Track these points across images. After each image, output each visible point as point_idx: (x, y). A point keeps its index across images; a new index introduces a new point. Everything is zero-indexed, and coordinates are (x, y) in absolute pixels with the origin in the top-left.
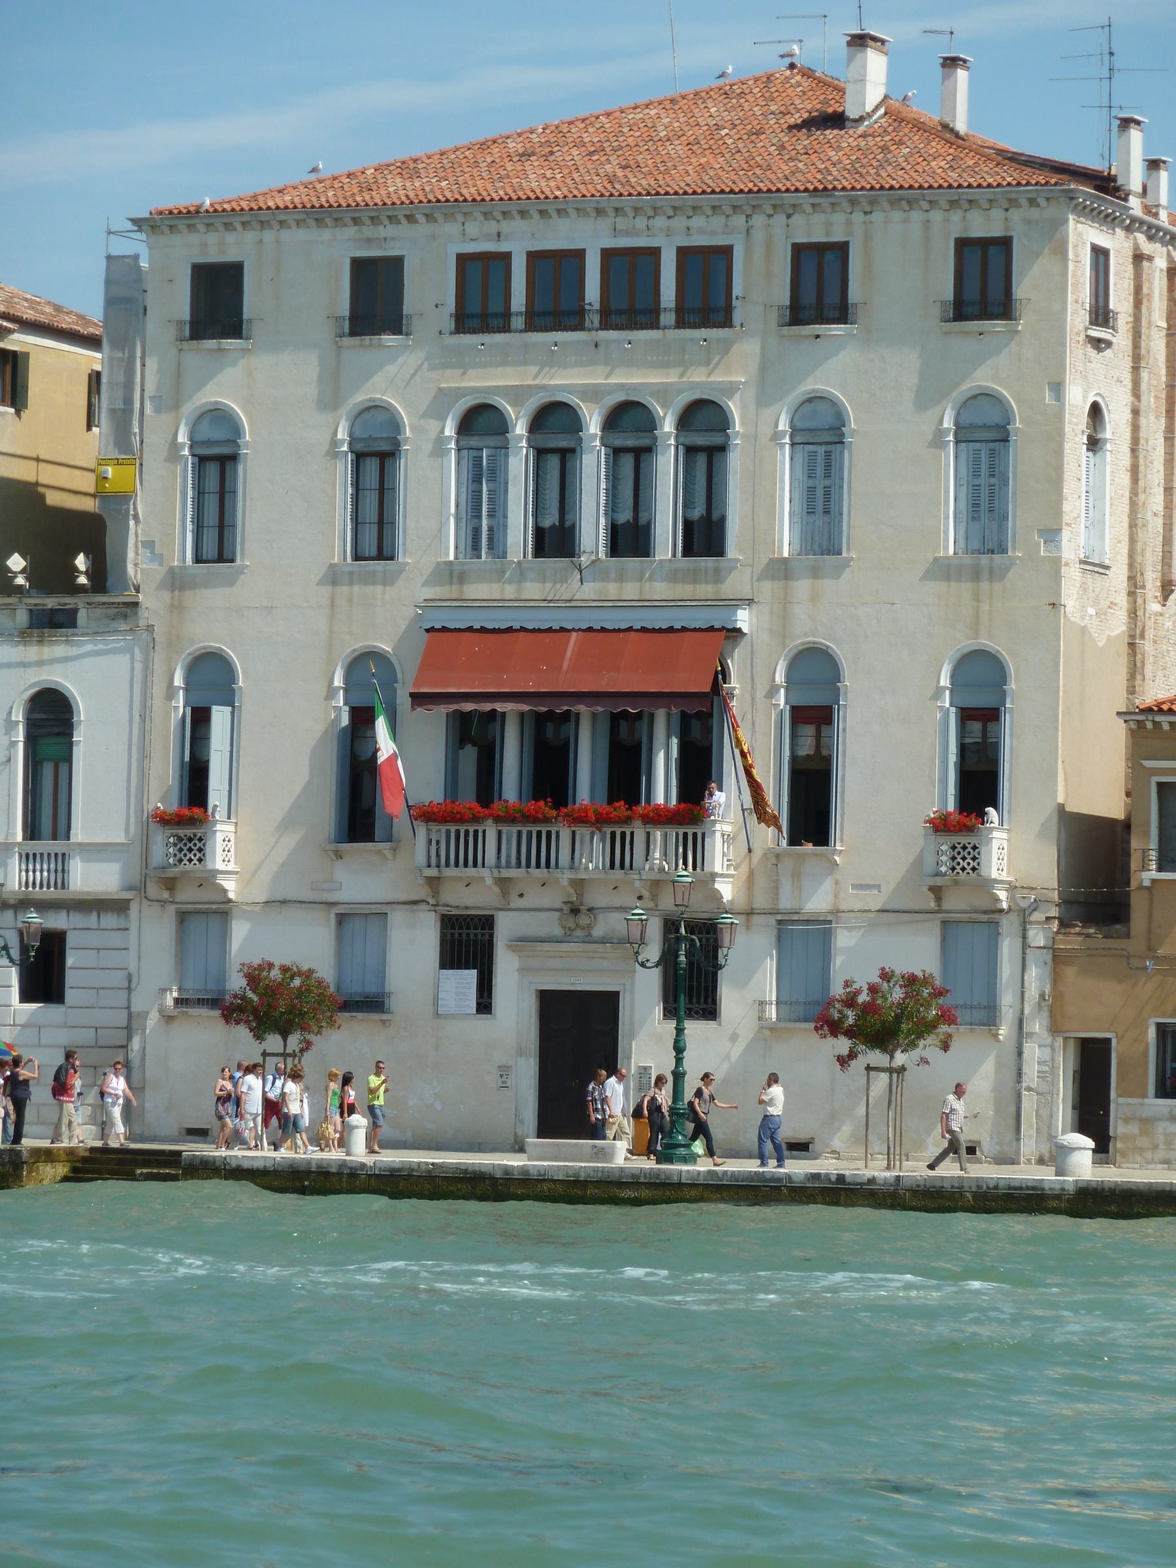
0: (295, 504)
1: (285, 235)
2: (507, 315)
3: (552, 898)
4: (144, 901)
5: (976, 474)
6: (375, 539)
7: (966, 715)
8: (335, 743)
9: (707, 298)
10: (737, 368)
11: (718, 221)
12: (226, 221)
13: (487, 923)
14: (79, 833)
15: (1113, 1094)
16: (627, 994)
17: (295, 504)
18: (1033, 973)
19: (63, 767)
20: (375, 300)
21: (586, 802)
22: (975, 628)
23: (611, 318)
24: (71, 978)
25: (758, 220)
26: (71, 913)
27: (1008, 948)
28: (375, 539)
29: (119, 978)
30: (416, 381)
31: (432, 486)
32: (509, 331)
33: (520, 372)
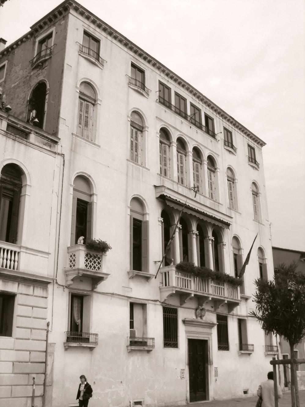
4: (55, 284)
8: (245, 291)
12: (252, 145)
16: (210, 341)
21: (238, 287)
24: (17, 321)
26: (20, 285)
29: (42, 324)
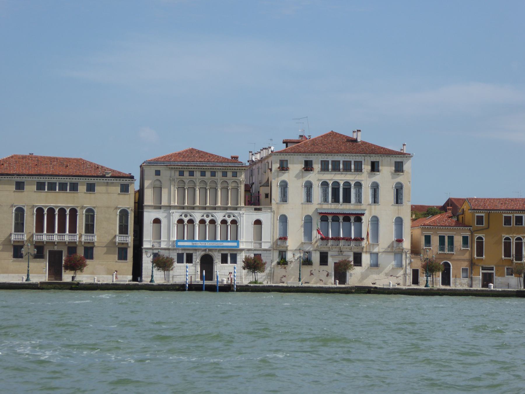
0: (296, 192)
6: (309, 198)
10: (366, 179)
11: (360, 158)
13: (327, 253)
17: (296, 192)
18: (407, 260)
22: (398, 214)
25: (366, 158)
27: (404, 256)
28: (309, 198)
31: (317, 192)
33: (330, 177)
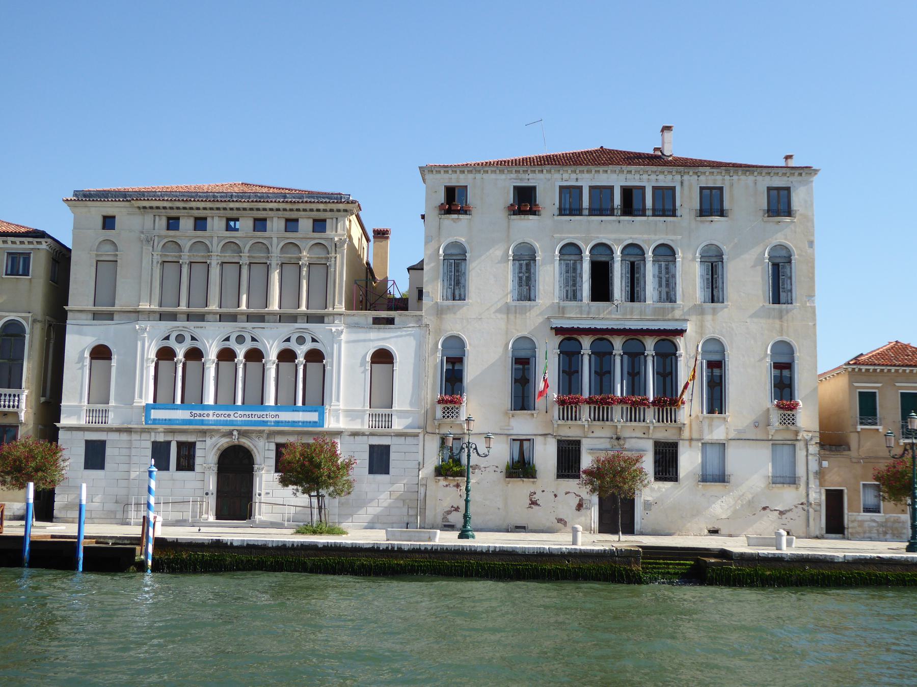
0: (491, 277)
1: (485, 176)
2: (613, 209)
3: (607, 433)
5: (660, 272)
7: (777, 366)
9: (666, 205)
13: (578, 443)
14: (396, 407)
15: (846, 511)
17: (491, 277)
19: (668, 379)
20: (524, 201)
23: (593, 212)
30: (546, 232)
32: (581, 215)
33: (589, 232)
